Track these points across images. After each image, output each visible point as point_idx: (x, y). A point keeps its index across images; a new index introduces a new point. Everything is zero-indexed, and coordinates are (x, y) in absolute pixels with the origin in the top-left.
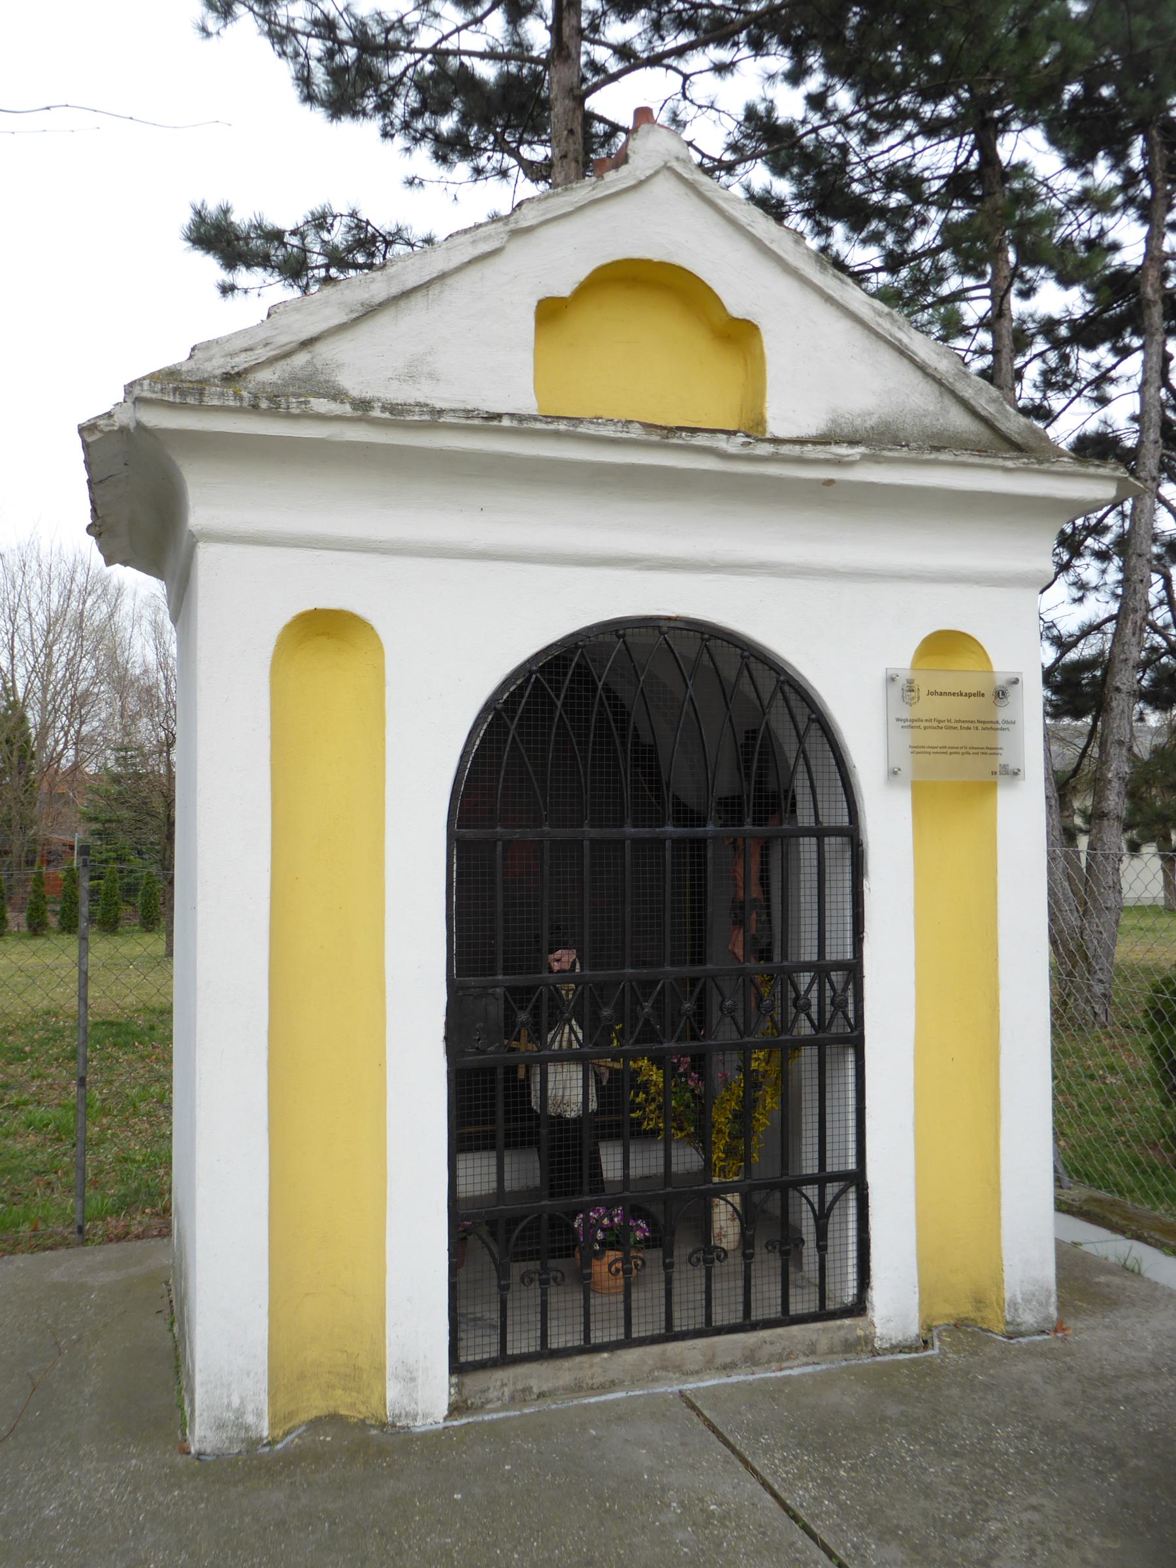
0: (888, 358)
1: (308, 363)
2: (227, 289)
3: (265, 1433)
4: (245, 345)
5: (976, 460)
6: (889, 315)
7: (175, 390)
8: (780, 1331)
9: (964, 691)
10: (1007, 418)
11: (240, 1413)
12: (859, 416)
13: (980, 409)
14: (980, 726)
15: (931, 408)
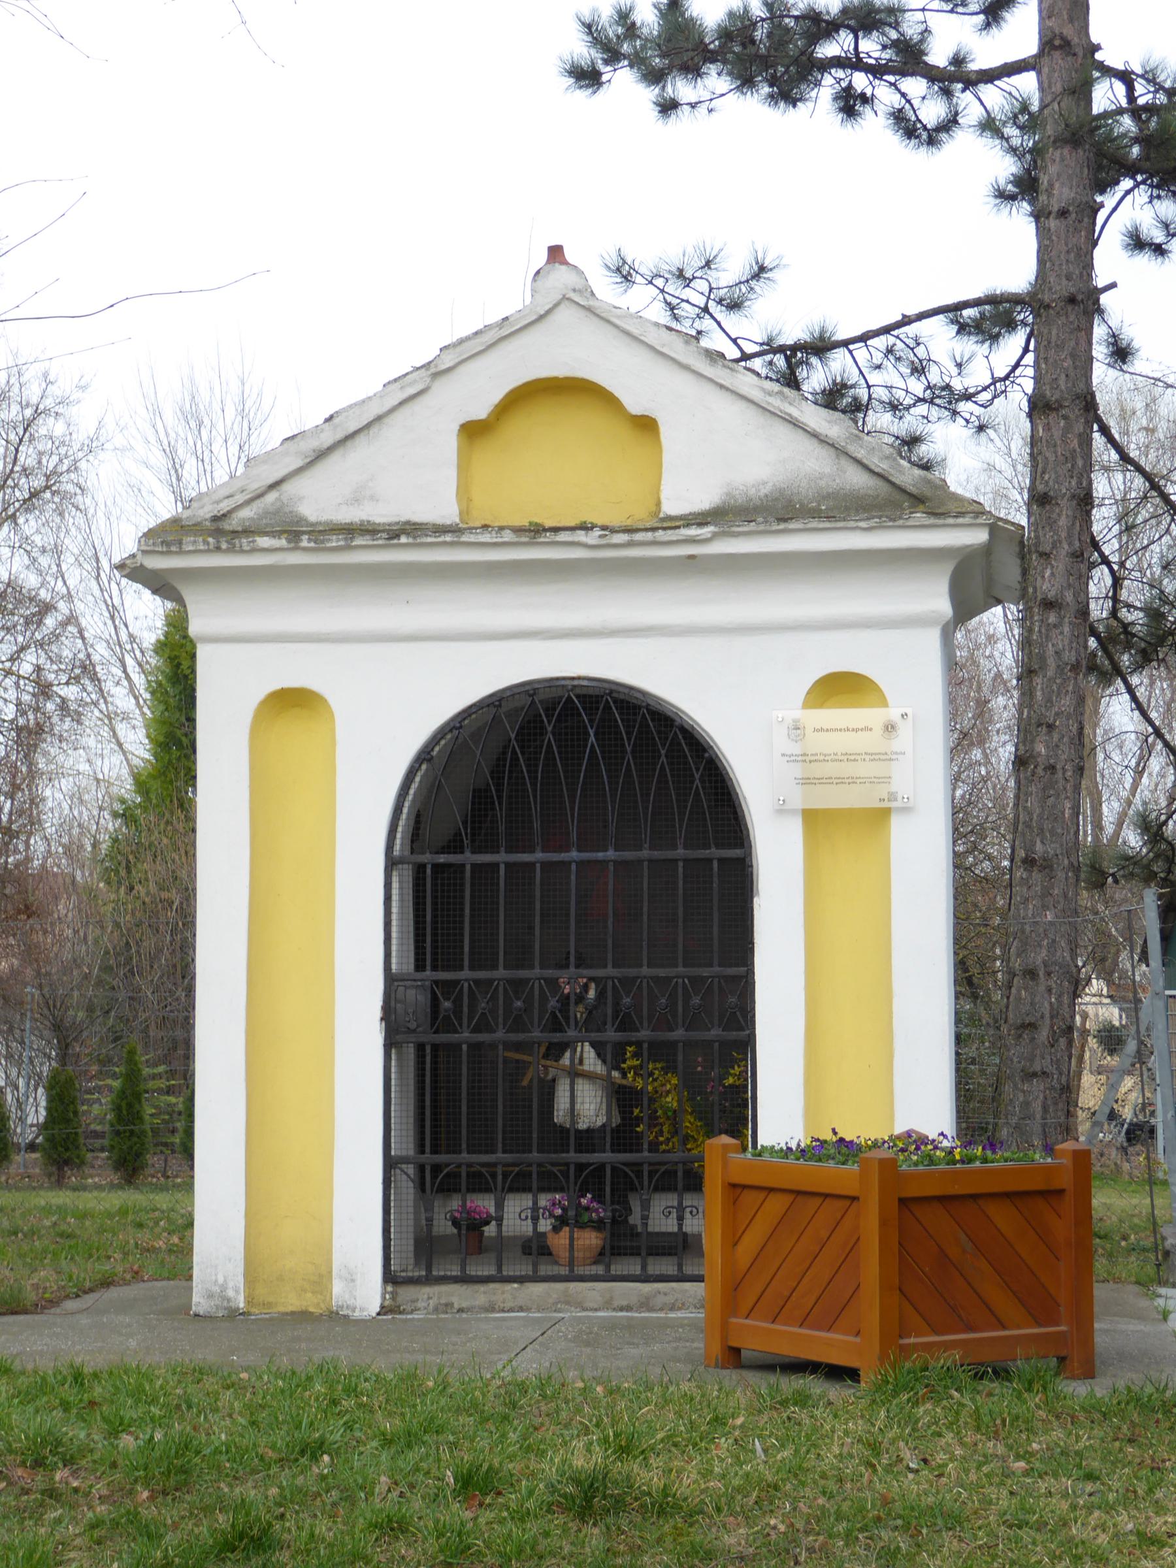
0: (783, 432)
1: (277, 499)
2: (668, 107)
3: (242, 1305)
4: (227, 494)
5: (828, 525)
6: (780, 393)
7: (162, 543)
8: (674, 1285)
9: (851, 727)
10: (902, 472)
11: (224, 1288)
12: (753, 486)
13: (873, 467)
14: (867, 757)
15: (827, 470)
